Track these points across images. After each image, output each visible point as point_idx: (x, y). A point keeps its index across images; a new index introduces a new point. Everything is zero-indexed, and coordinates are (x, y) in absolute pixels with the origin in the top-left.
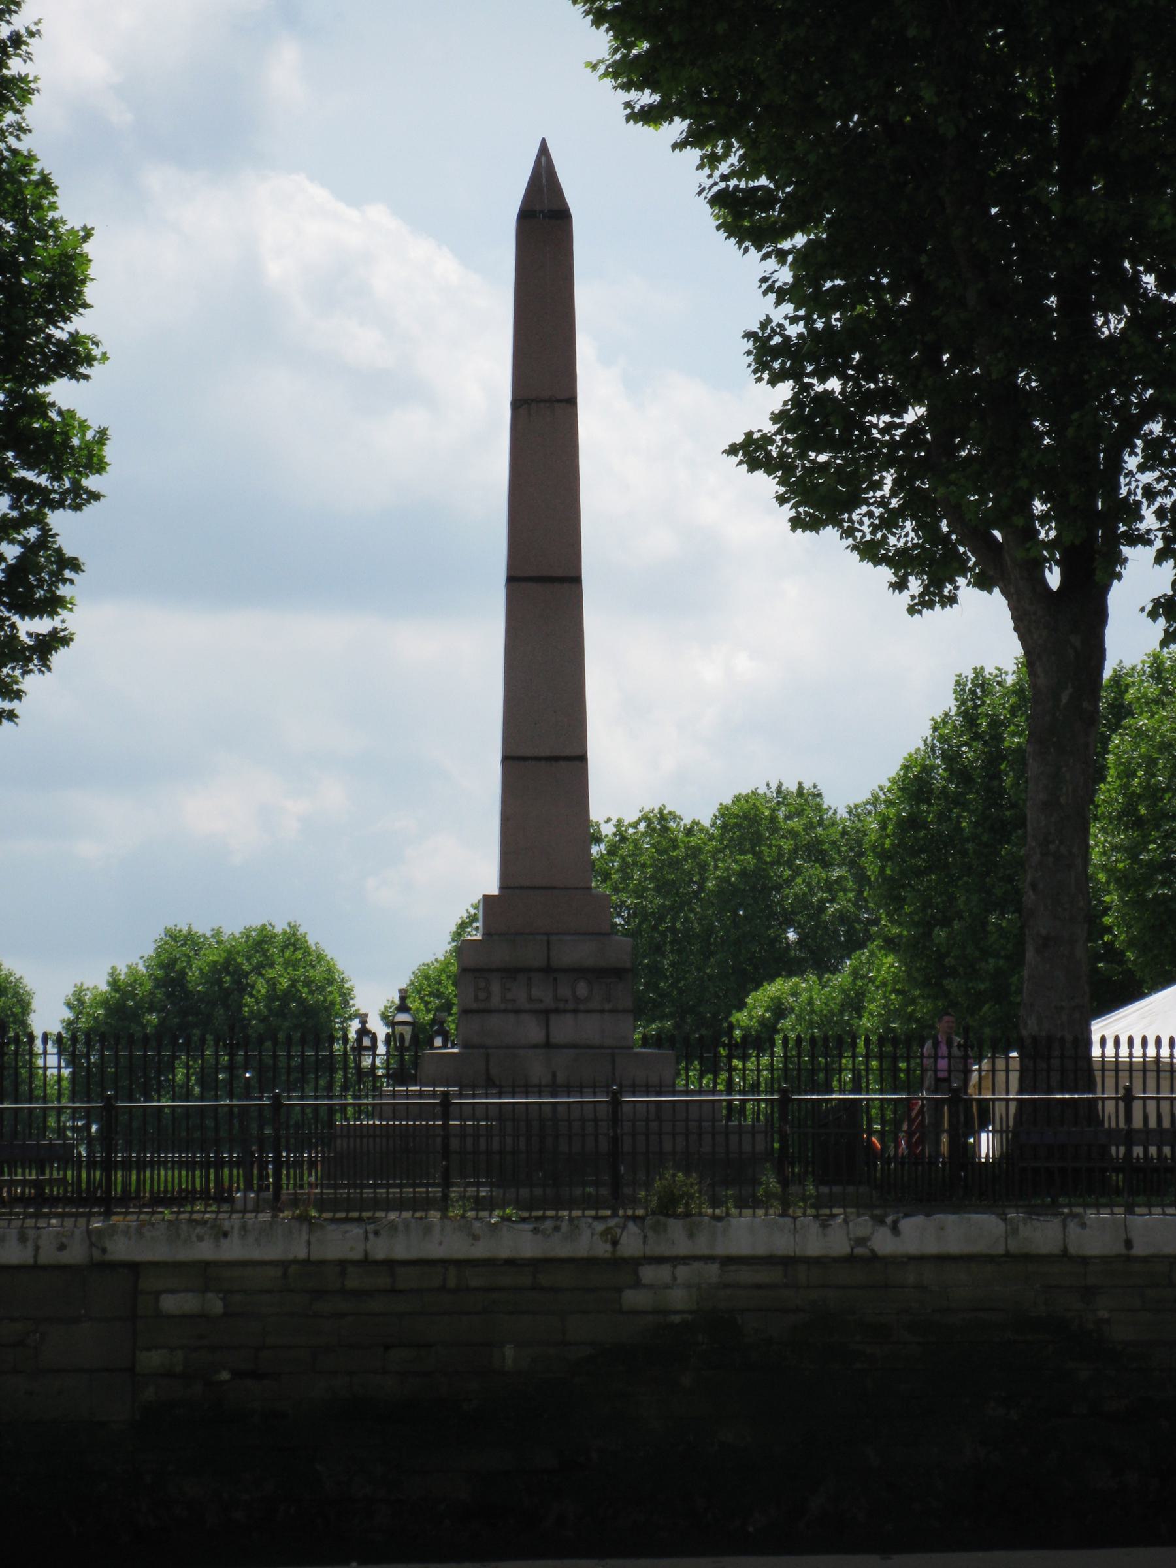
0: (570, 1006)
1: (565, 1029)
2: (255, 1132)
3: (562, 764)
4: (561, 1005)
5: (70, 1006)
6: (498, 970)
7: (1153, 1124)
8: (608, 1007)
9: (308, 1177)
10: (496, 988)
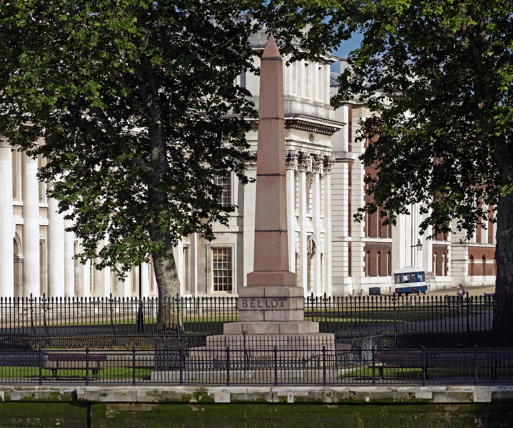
0: (271, 309)
1: (269, 315)
2: (301, 365)
3: (272, 232)
4: (268, 308)
5: (257, 32)
6: (250, 298)
7: (456, 330)
8: (282, 308)
9: (449, 411)
10: (249, 303)
